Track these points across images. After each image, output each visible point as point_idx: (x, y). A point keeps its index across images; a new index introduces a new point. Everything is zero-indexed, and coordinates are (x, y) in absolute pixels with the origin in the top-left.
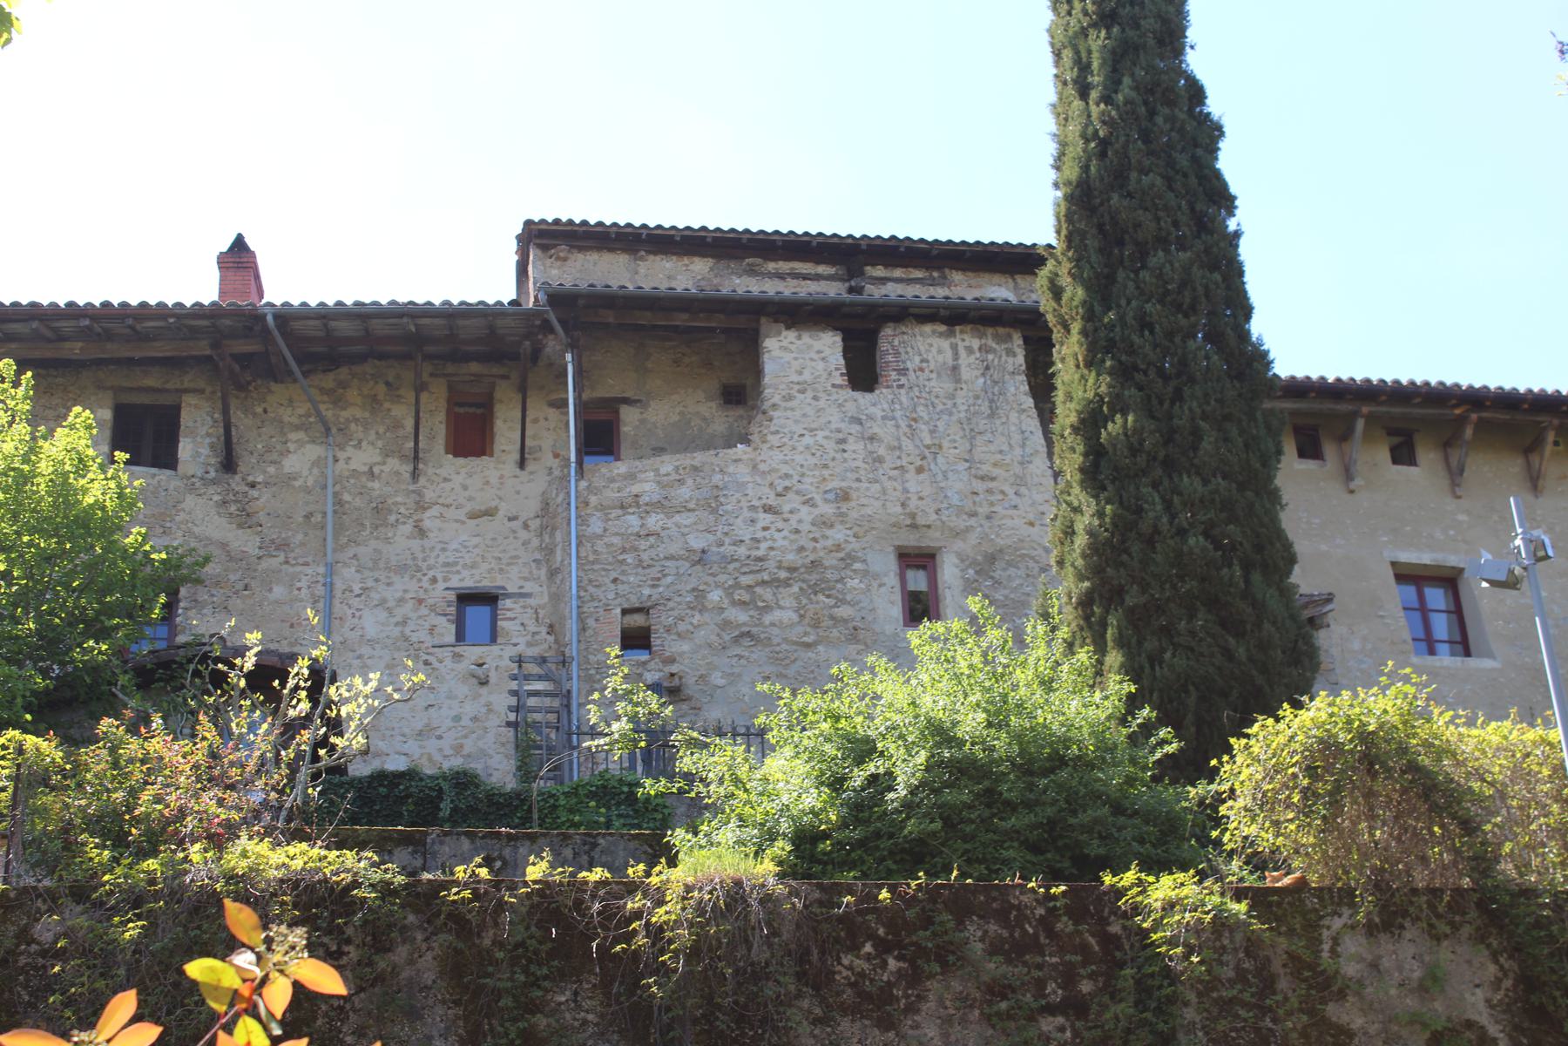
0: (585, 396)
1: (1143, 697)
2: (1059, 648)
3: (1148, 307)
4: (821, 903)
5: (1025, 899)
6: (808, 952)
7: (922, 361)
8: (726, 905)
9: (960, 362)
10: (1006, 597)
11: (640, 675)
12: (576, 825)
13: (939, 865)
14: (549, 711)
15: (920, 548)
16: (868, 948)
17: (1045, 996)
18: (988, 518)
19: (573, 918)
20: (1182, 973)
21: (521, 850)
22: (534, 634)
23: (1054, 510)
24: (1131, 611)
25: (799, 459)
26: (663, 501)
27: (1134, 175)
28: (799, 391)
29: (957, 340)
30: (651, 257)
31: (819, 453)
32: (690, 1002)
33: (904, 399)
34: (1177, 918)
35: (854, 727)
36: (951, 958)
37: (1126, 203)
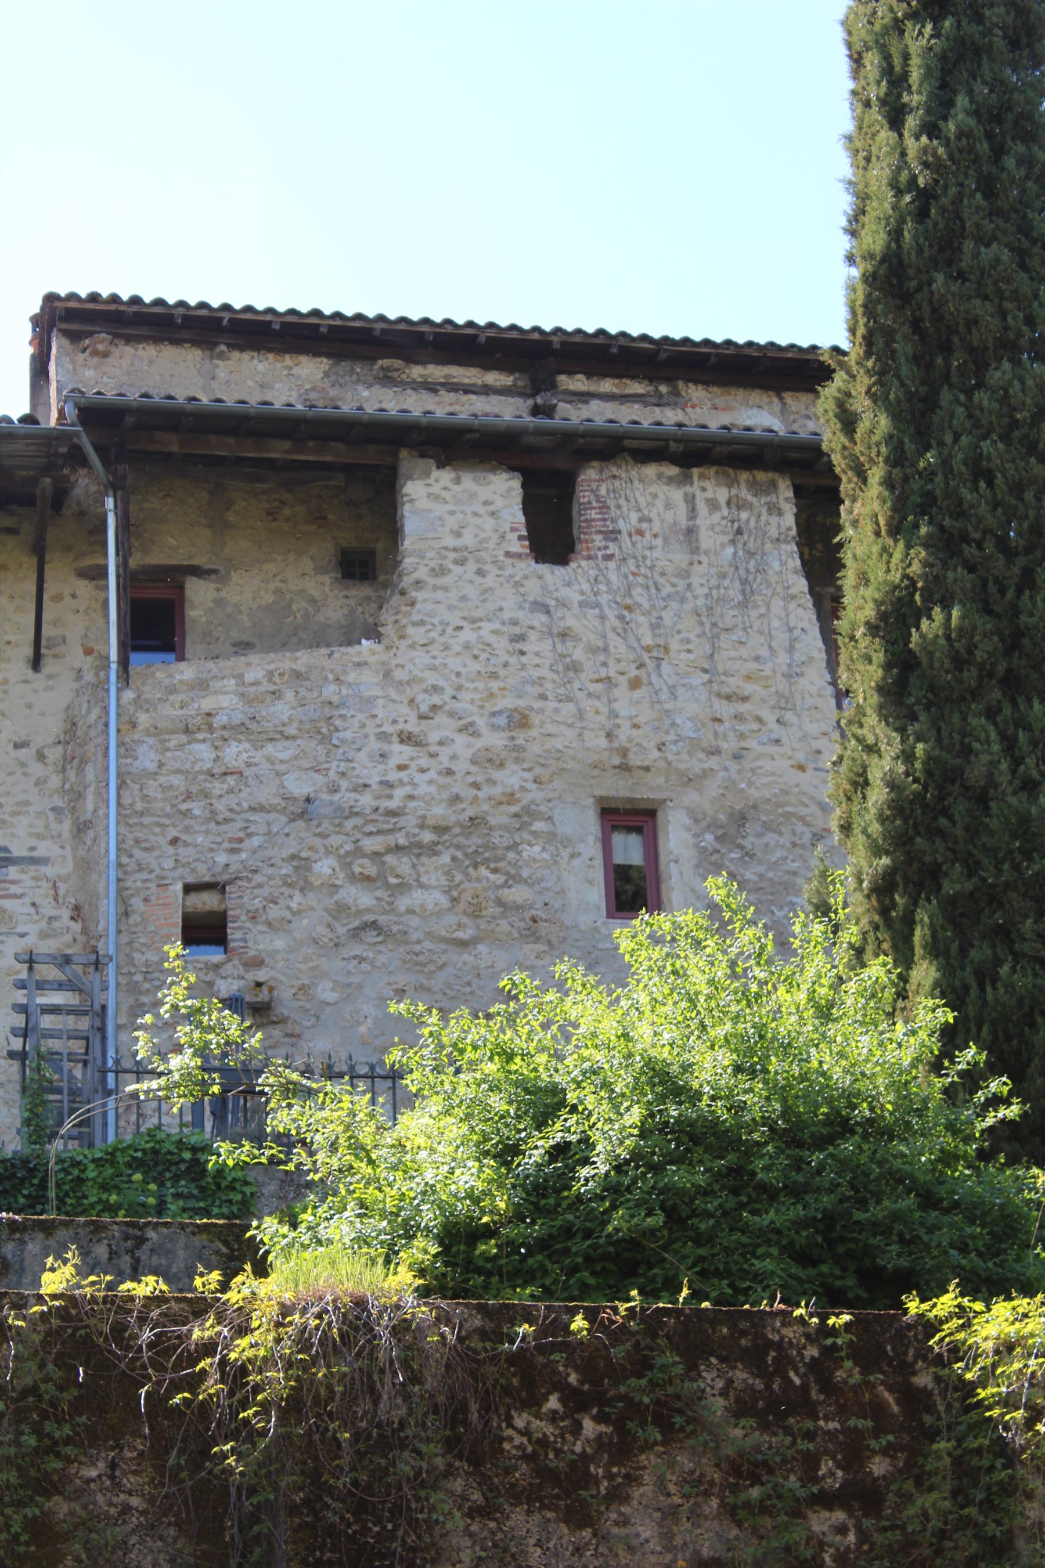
0: (133, 563)
1: (968, 1031)
2: (843, 955)
3: (985, 445)
4: (483, 1334)
5: (788, 1333)
6: (464, 1408)
7: (641, 520)
8: (342, 1335)
9: (698, 522)
10: (761, 876)
11: (210, 984)
12: (112, 1209)
13: (660, 1280)
14: (73, 1036)
15: (631, 800)
16: (553, 1403)
17: (816, 1480)
18: (737, 757)
19: (110, 1351)
20: (1023, 1450)
21: (30, 1246)
22: (51, 919)
23: (838, 749)
24: (950, 904)
25: (454, 663)
26: (248, 723)
27: (968, 245)
28: (456, 562)
29: (695, 489)
30: (236, 354)
31: (484, 656)
32: (285, 1481)
33: (613, 577)
34: (1017, 1366)
35: (535, 1070)
36: (678, 1420)
37: (955, 287)
